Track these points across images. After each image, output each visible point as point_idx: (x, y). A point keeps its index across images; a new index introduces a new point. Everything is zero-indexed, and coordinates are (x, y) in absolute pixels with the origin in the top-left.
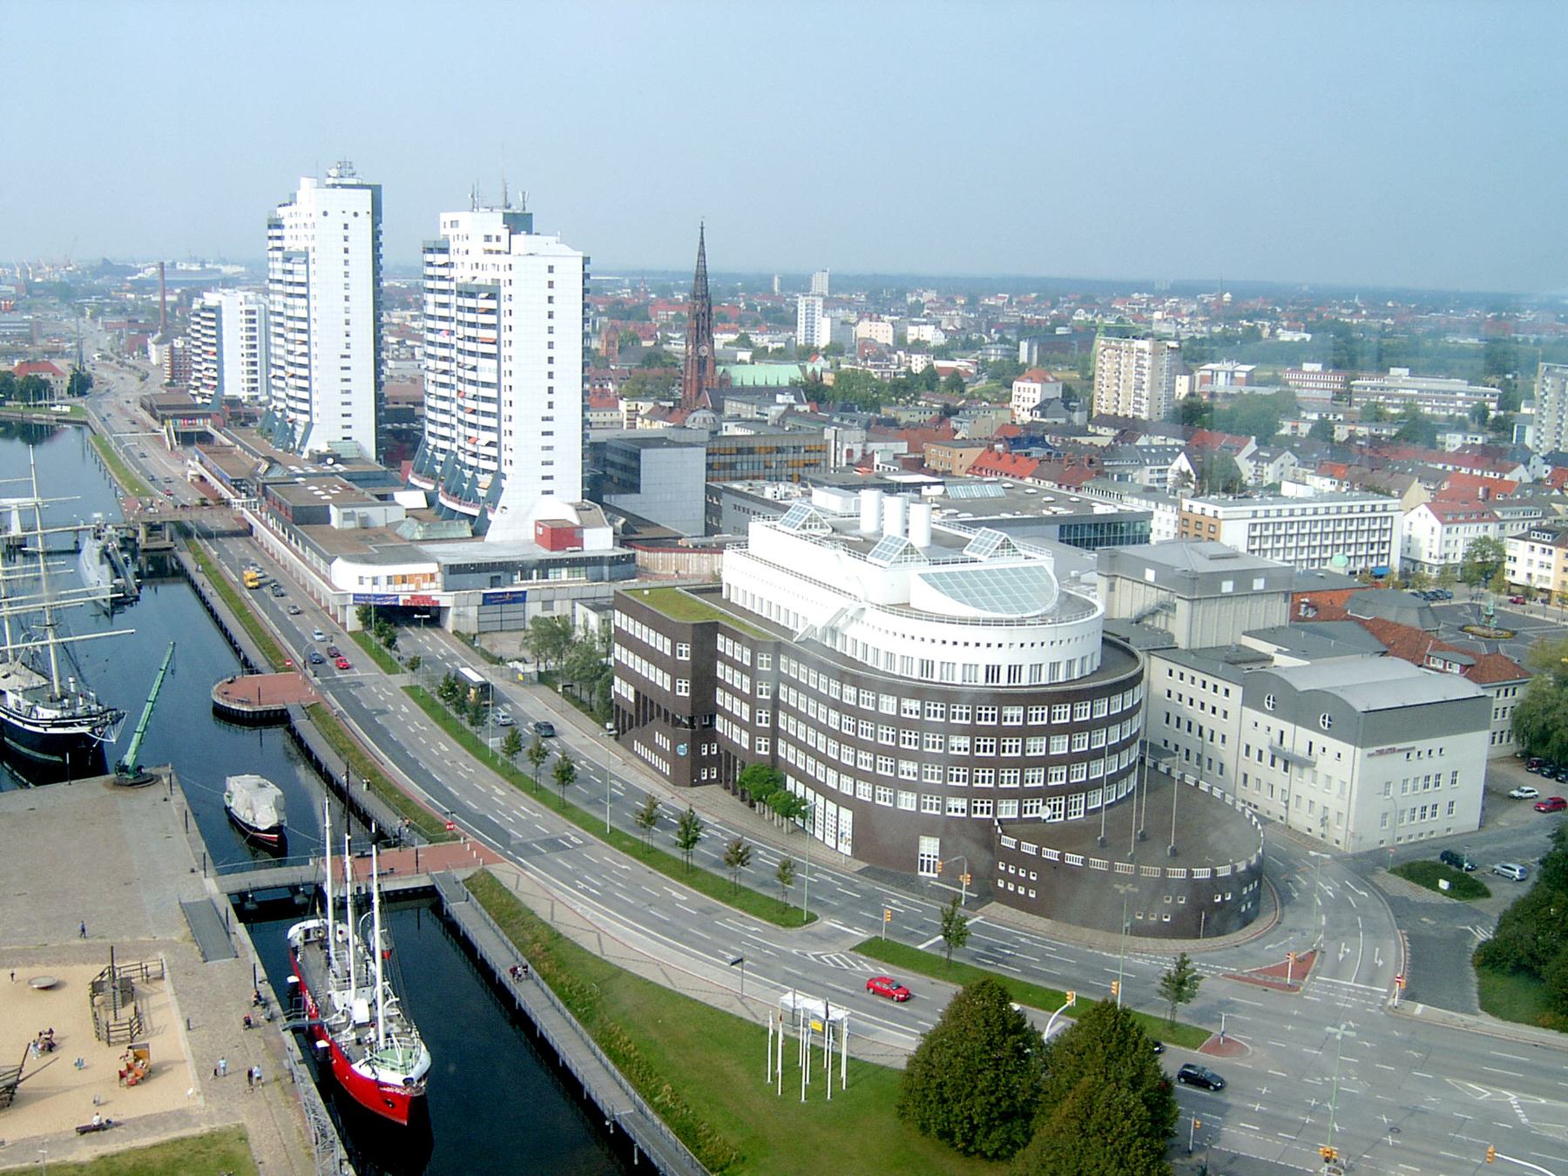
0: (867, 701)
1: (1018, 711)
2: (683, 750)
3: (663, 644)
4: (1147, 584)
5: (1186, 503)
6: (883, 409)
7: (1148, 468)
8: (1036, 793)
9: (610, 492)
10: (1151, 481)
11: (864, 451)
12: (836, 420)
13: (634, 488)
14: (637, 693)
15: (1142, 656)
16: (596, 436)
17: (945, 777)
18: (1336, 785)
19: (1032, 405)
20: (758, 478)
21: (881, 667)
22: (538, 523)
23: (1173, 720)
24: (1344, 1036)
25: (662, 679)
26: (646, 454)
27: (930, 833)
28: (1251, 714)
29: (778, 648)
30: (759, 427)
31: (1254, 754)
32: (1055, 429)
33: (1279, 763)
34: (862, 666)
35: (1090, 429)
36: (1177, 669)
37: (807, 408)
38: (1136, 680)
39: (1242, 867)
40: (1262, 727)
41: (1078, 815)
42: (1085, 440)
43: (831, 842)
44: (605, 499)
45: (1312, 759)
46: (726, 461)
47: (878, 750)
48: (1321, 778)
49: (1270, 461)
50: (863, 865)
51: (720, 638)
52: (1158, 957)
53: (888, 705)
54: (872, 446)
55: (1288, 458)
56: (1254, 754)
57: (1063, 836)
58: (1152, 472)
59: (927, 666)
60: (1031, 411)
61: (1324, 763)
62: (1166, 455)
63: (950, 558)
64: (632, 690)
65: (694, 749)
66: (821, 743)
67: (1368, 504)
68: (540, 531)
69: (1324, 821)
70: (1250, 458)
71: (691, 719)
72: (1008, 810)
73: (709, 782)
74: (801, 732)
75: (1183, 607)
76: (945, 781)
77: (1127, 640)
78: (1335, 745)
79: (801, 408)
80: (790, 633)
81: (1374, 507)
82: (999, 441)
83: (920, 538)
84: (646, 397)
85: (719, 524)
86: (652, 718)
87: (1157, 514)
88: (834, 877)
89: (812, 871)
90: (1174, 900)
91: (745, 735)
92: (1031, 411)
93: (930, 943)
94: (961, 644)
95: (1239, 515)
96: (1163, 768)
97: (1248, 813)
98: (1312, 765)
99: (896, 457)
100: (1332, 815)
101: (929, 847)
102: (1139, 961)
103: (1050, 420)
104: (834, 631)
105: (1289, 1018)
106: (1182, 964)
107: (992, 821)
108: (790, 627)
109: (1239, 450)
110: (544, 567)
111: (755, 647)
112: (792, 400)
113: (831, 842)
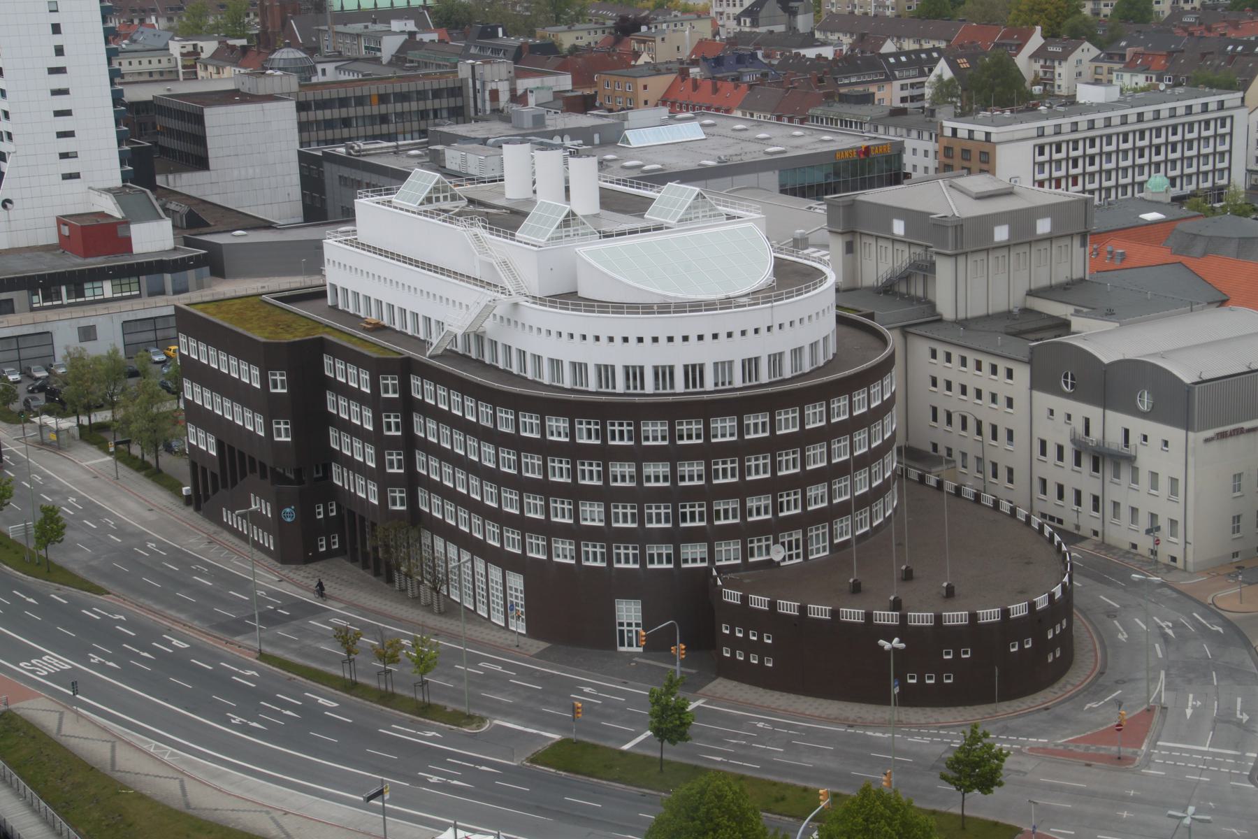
0: (529, 426)
1: (730, 423)
2: (289, 514)
3: (249, 375)
4: (895, 241)
5: (948, 125)
6: (539, 31)
7: (897, 84)
8: (762, 529)
9: (167, 171)
10: (903, 100)
11: (513, 91)
12: (473, 51)
13: (201, 163)
14: (220, 445)
15: (893, 337)
16: (135, 94)
17: (677, 517)
18: (1164, 483)
19: (738, 10)
20: (358, 138)
21: (546, 380)
22: (61, 221)
23: (942, 416)
24: (1185, 811)
25: (252, 422)
26: (214, 117)
27: (629, 594)
28: (1044, 400)
29: (406, 368)
30: (370, 69)
31: (1052, 450)
32: (771, 40)
33: (1087, 463)
34: (522, 380)
35: (818, 35)
36: (941, 350)
37: (435, 36)
38: (885, 367)
39: (1042, 602)
40: (1060, 416)
41: (819, 553)
42: (810, 53)
43: (498, 620)
44: (160, 180)
45: (1131, 451)
46: (321, 115)
47: (546, 489)
48: (1144, 478)
49: (1063, 57)
50: (543, 645)
51: (327, 361)
52: (934, 734)
53: (558, 429)
54: (523, 84)
55: (1087, 51)
56: (1052, 450)
57: (803, 578)
58: (903, 87)
59: (694, 373)
60: (737, 19)
61: (1147, 459)
62: (921, 63)
63: (626, 227)
64: (212, 440)
65: (306, 513)
66: (474, 488)
67: (1196, 103)
68: (66, 231)
69: (1153, 529)
70: (1035, 56)
71: (298, 472)
72: (729, 554)
73: (330, 554)
74: (447, 476)
75: (944, 268)
76: (676, 523)
77: (871, 316)
78: (1158, 431)
79: (426, 37)
80: (422, 344)
81: (1205, 105)
82: (694, 63)
83: (585, 202)
84: (208, 35)
85: (324, 198)
86: (244, 475)
87: (909, 144)
88: (505, 666)
89: (474, 660)
90: (957, 655)
91: (373, 488)
92: (737, 19)
93: (638, 740)
94: (693, 338)
95: (1017, 136)
96: (932, 480)
97: (1047, 530)
98: (1131, 459)
99: (558, 95)
100: (1163, 522)
101: (629, 612)
102: (917, 739)
103: (762, 30)
104: (480, 338)
105: (1123, 801)
106: (974, 738)
107: (707, 571)
108: (422, 336)
109: (1019, 47)
110: (77, 281)
111: (378, 367)
112: (411, 26)
113: (498, 620)
